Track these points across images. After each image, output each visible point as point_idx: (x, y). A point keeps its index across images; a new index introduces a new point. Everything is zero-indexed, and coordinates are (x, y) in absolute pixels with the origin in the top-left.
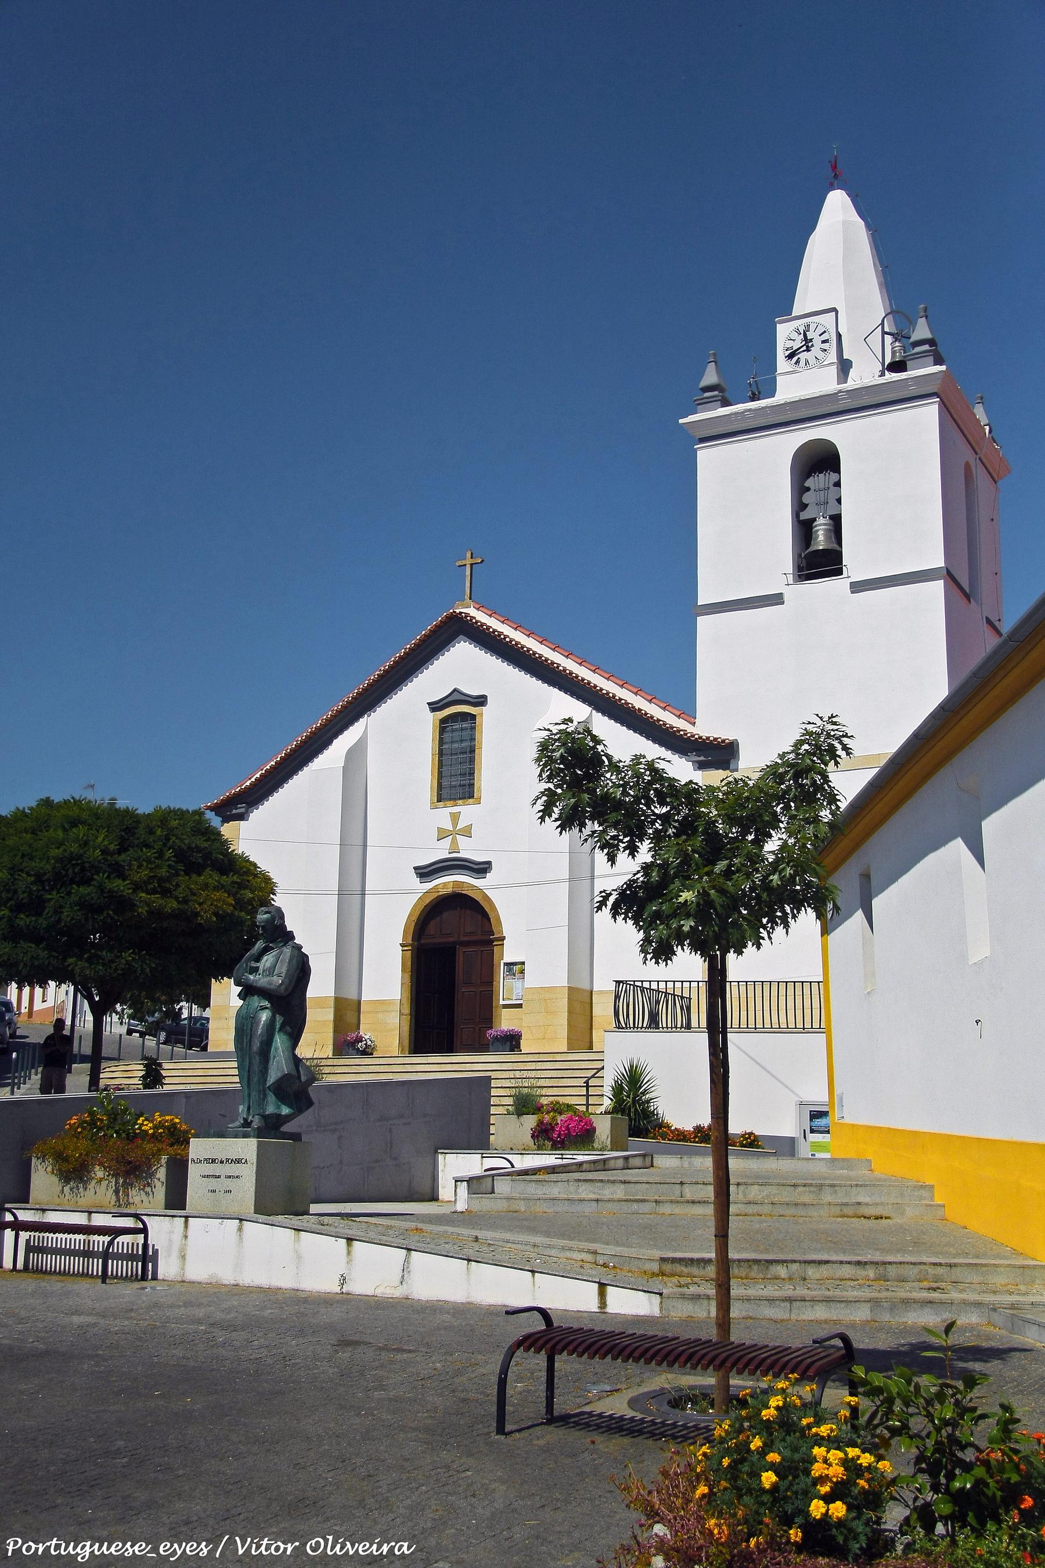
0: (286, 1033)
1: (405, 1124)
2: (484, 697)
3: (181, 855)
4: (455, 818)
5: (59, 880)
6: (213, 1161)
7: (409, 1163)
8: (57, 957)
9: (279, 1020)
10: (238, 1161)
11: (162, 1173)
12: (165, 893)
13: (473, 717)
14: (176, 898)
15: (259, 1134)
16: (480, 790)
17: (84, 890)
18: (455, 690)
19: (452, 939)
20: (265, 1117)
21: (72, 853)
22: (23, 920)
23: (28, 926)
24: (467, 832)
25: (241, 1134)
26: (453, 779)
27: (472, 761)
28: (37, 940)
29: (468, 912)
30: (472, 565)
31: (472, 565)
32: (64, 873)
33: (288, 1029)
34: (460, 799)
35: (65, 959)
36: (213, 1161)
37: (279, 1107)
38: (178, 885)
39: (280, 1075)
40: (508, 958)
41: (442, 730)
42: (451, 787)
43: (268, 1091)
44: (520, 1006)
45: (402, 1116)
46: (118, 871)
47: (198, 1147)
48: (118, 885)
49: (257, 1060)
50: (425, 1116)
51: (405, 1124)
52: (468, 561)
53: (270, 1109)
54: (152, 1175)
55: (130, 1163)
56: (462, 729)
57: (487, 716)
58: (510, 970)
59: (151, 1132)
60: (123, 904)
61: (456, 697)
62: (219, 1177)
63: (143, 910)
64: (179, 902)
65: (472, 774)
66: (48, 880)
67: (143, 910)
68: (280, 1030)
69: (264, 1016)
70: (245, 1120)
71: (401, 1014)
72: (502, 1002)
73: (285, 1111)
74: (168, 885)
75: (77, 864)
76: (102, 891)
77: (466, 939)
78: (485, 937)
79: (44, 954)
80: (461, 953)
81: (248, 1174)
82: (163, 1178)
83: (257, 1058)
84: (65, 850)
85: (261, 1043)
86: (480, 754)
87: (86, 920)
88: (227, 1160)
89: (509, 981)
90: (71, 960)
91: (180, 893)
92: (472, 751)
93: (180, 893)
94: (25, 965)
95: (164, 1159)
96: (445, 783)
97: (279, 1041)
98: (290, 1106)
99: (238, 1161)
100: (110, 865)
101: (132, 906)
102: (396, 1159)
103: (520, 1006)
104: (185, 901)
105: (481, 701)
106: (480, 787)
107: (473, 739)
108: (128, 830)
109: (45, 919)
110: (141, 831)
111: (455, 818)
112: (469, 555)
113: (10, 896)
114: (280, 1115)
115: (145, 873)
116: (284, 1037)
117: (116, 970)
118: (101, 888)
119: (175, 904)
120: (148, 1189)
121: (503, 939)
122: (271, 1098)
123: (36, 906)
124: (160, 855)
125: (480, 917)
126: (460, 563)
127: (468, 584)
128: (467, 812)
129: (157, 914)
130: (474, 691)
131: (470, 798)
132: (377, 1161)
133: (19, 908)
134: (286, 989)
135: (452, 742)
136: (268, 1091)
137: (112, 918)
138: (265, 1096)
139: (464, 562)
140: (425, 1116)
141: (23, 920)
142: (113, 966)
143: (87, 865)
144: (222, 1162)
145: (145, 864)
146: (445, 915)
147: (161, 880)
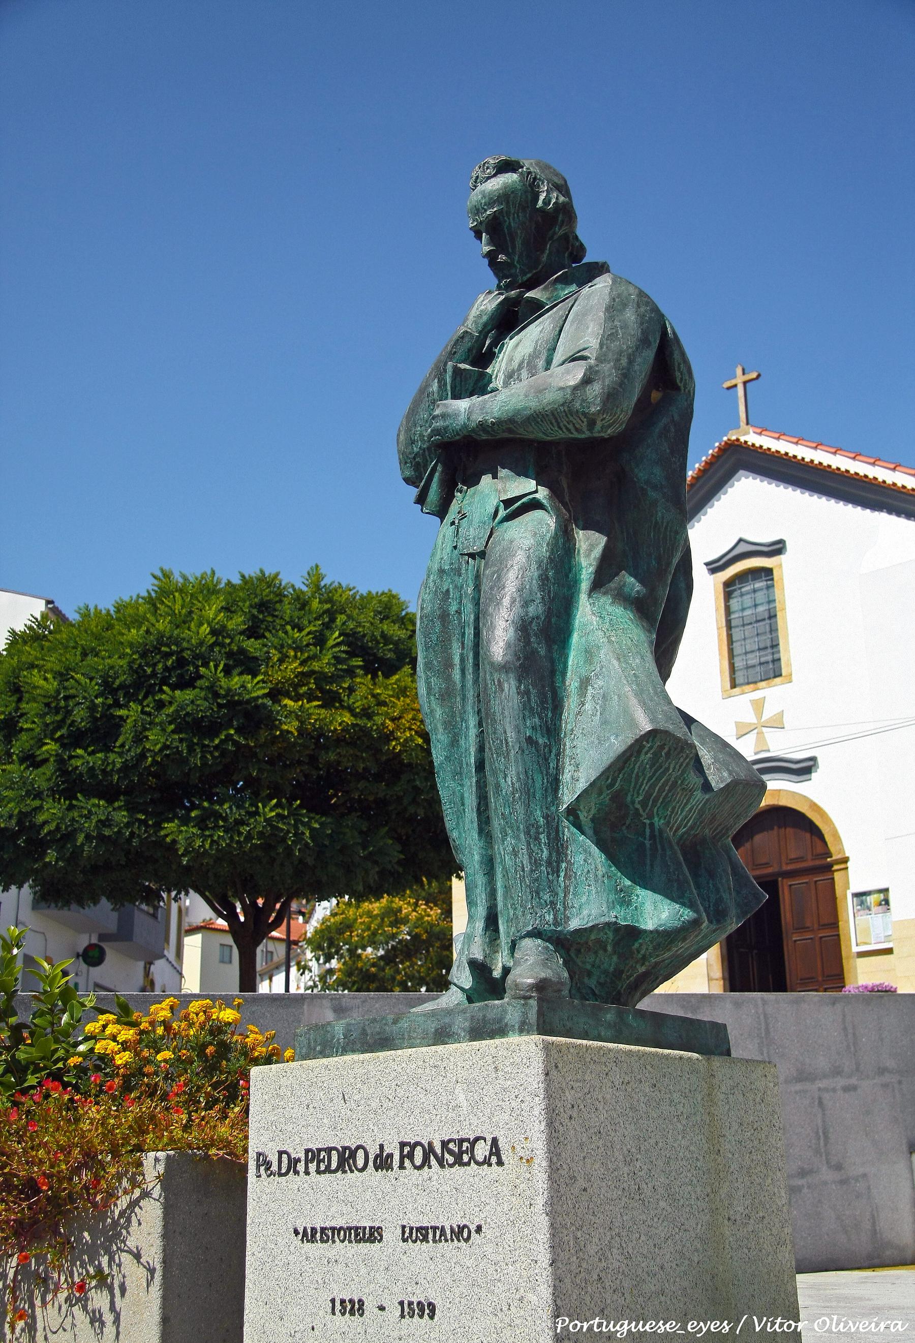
0: (621, 597)
1: (846, 1089)
2: (781, 542)
3: (355, 644)
4: (758, 706)
5: (140, 685)
6: (347, 1159)
7: (865, 1175)
8: (144, 822)
9: (589, 546)
10: (458, 1152)
11: (147, 1230)
12: (331, 701)
13: (768, 572)
14: (351, 710)
15: (551, 1012)
16: (789, 665)
17: (184, 696)
18: (740, 540)
19: (770, 870)
20: (565, 944)
21: (161, 635)
22: (83, 759)
23: (92, 769)
24: (777, 723)
25: (460, 1024)
26: (750, 656)
27: (773, 630)
28: (109, 794)
29: (790, 831)
30: (745, 383)
31: (745, 383)
32: (149, 671)
33: (631, 583)
34: (762, 680)
35: (158, 826)
36: (347, 1159)
37: (624, 900)
38: (351, 690)
39: (617, 744)
40: (856, 886)
41: (728, 596)
42: (748, 667)
43: (568, 831)
44: (889, 951)
45: (837, 1072)
46: (247, 664)
47: (286, 1103)
48: (252, 687)
49: (508, 697)
50: (882, 1071)
51: (846, 1089)
52: (739, 379)
53: (588, 908)
54: (112, 1236)
55: (31, 1187)
56: (755, 591)
57: (785, 567)
58: (862, 903)
59: (122, 1059)
60: (253, 717)
61: (744, 550)
62: (373, 1235)
63: (291, 726)
64: (354, 715)
65: (775, 646)
66: (122, 686)
67: (291, 726)
68: (598, 584)
69: (529, 536)
70: (479, 969)
71: (710, 979)
72: (855, 949)
73: (656, 912)
74: (334, 687)
75: (170, 654)
76: (216, 695)
77: (789, 867)
78: (818, 863)
79: (121, 816)
80: (785, 887)
81: (512, 1206)
82: (153, 1254)
83: (510, 686)
84: (148, 632)
85: (523, 627)
86: (785, 619)
87: (191, 749)
88: (407, 1150)
89: (863, 918)
90: (170, 826)
91: (358, 700)
92: (772, 616)
93: (358, 700)
94: (88, 837)
95: (153, 1164)
96: (739, 663)
97: (600, 627)
98: (671, 890)
99: (458, 1152)
100: (230, 655)
101: (270, 721)
102: (839, 1167)
103: (889, 951)
104: (367, 713)
105: (777, 548)
106: (788, 660)
107: (771, 601)
108: (264, 606)
109: (120, 754)
110: (287, 610)
111: (758, 706)
112: (739, 371)
113: (58, 718)
114: (633, 932)
115: (293, 667)
116: (622, 615)
117: (249, 837)
118: (213, 691)
119: (347, 718)
120: (99, 1300)
121: (845, 860)
122: (586, 855)
123: (103, 731)
124: (320, 640)
125: (808, 835)
126: (728, 384)
127: (742, 408)
128: (773, 694)
129: (316, 738)
130: (766, 537)
131: (775, 677)
132: (803, 1173)
133: (76, 739)
134: (611, 397)
135: (743, 610)
136: (568, 831)
137: (235, 743)
138: (558, 849)
139: (733, 382)
140: (882, 1071)
141: (83, 759)
142: (245, 829)
143: (187, 654)
144: (383, 1162)
145: (292, 653)
146: (758, 838)
147: (321, 678)
